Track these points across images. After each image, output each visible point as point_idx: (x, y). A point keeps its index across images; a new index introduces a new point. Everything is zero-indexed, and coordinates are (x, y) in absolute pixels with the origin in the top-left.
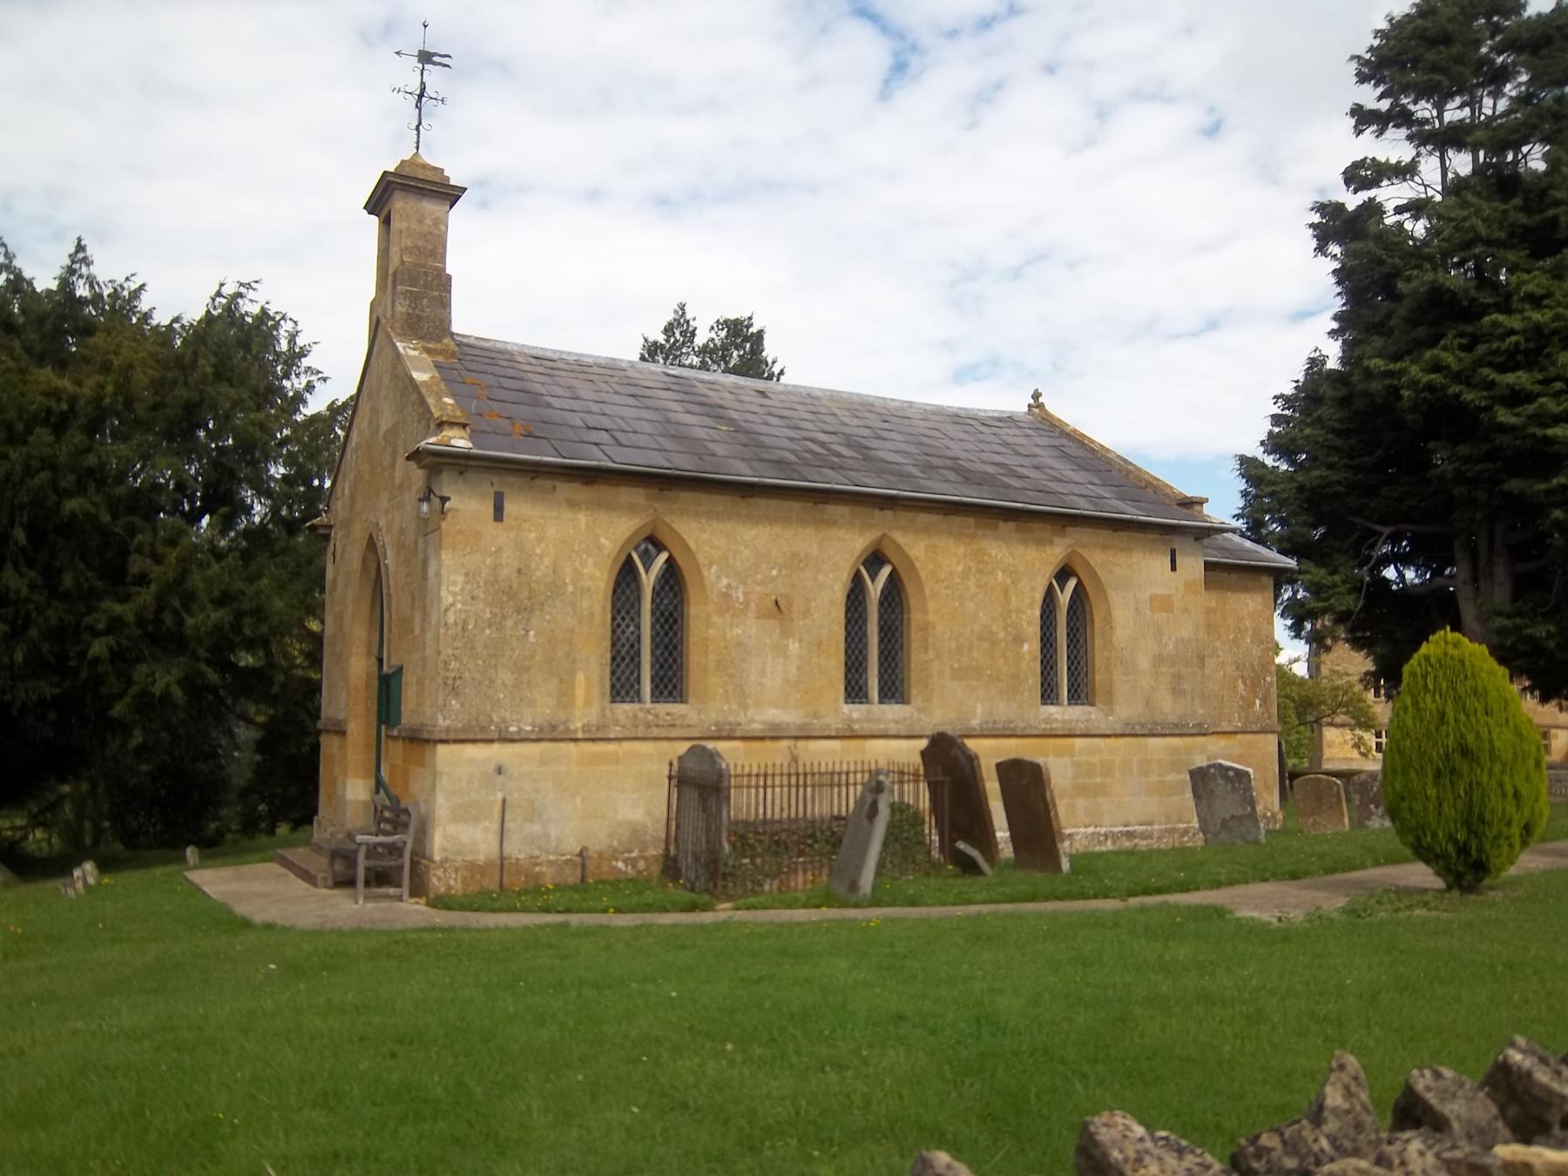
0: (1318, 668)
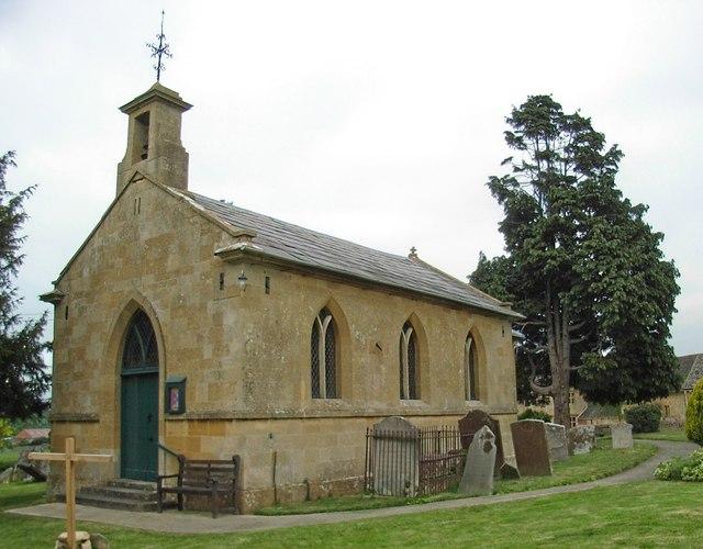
0: (68, 331)
